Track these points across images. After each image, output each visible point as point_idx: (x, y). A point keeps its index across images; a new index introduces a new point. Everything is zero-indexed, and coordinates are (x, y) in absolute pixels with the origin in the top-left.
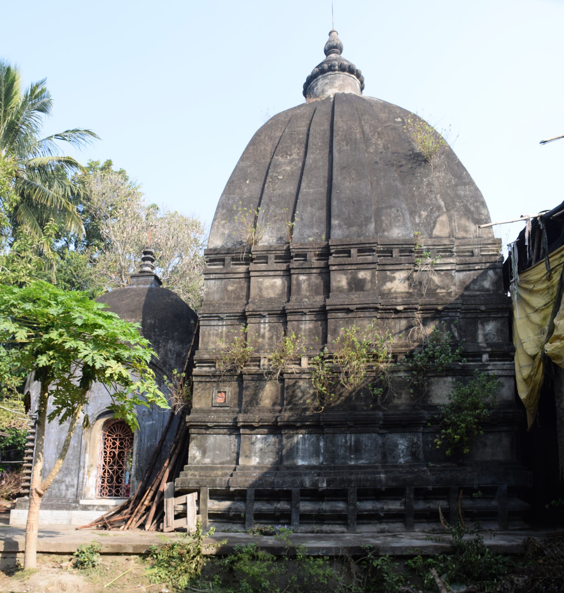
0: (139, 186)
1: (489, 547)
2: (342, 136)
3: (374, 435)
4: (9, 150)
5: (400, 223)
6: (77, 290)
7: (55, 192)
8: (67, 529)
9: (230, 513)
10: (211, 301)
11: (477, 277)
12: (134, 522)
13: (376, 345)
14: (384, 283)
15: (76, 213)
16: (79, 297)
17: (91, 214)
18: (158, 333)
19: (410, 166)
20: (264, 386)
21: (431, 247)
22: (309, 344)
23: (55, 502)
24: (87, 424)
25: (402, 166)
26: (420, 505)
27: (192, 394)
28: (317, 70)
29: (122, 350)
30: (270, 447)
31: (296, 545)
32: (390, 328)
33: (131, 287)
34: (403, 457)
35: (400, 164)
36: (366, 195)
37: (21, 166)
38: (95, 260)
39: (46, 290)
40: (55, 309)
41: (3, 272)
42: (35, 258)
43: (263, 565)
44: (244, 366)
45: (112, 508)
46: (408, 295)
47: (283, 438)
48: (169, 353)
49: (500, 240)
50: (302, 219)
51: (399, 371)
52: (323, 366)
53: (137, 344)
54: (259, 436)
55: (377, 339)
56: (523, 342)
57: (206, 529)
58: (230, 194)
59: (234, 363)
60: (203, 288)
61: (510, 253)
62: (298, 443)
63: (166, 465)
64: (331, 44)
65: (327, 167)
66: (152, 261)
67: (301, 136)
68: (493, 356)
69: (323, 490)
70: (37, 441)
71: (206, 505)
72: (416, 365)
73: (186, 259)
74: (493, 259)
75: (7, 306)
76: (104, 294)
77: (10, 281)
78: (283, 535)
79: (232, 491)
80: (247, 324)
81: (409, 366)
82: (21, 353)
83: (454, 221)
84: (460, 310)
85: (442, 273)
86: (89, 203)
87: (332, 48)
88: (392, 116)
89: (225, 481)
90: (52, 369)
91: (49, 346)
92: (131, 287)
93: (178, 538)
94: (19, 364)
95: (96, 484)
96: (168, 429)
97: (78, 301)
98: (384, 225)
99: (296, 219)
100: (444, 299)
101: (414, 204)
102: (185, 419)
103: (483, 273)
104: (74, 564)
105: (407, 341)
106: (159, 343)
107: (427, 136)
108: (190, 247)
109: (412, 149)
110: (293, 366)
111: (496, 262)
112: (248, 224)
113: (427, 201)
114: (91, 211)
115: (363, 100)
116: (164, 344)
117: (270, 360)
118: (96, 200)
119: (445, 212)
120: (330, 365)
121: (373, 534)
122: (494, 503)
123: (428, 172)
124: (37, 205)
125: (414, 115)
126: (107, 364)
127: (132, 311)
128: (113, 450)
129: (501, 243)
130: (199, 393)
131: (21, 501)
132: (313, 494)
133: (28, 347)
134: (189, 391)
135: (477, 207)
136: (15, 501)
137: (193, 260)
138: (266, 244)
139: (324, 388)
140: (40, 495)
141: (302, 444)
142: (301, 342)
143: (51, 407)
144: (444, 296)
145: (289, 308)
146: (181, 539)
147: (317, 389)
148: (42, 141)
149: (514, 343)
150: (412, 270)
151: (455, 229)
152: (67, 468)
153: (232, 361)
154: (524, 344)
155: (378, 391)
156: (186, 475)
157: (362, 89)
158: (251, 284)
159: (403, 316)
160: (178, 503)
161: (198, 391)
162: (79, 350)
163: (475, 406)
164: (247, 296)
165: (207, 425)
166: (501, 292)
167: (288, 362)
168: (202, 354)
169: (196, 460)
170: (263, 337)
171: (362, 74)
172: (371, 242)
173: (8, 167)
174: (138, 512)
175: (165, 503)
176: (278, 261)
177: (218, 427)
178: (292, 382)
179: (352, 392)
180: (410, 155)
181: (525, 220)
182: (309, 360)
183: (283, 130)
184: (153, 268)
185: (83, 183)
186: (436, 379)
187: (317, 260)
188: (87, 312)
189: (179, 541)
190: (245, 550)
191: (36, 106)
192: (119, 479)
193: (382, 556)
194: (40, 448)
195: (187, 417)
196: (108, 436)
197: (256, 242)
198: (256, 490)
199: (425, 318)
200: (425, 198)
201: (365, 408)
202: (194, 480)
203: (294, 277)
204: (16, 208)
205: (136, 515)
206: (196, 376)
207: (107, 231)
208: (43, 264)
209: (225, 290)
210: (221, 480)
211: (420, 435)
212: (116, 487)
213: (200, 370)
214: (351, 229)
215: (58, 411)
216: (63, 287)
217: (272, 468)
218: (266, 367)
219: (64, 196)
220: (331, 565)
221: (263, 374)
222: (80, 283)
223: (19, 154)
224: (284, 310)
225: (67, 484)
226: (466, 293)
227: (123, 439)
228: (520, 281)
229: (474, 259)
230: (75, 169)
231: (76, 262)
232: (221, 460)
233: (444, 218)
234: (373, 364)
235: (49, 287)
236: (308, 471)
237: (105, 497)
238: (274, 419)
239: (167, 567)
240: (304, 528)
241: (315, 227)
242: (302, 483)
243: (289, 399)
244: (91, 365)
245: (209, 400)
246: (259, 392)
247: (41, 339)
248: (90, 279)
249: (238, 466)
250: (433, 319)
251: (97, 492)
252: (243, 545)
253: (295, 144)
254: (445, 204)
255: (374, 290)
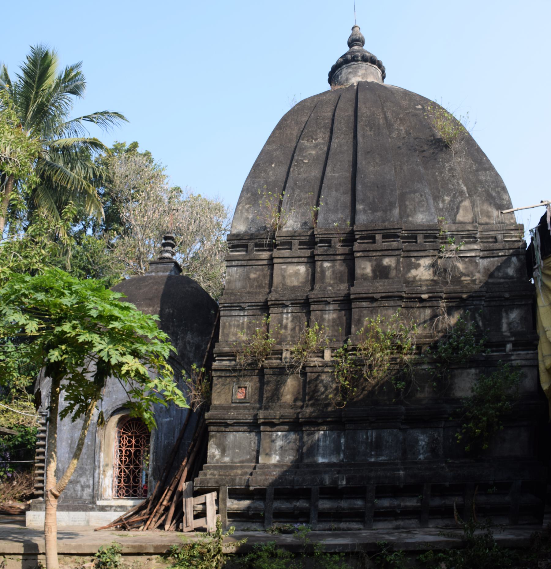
0: (163, 169)
1: (498, 541)
2: (365, 121)
3: (395, 430)
4: (35, 131)
5: (424, 208)
6: (92, 278)
7: (77, 174)
8: (86, 531)
9: (250, 512)
10: (232, 290)
11: (501, 264)
12: (153, 523)
13: (401, 335)
14: (409, 271)
15: (97, 195)
16: (94, 286)
17: (112, 196)
18: (176, 324)
19: (431, 151)
20: (286, 381)
21: (455, 233)
22: (332, 336)
23: (71, 503)
24: (102, 422)
25: (424, 151)
26: (436, 502)
27: (211, 390)
28: (341, 60)
29: (138, 345)
30: (291, 444)
31: (314, 542)
32: (415, 318)
33: (150, 274)
34: (422, 454)
35: (422, 149)
36: (390, 180)
37: (44, 147)
38: (113, 246)
39: (60, 278)
40: (69, 299)
41: (15, 259)
42: (50, 243)
43: (282, 562)
44: (266, 359)
45: (130, 509)
46: (433, 283)
47: (304, 435)
48: (187, 345)
49: (522, 225)
50: (327, 204)
51: (423, 363)
52: (346, 358)
53: (156, 337)
54: (279, 433)
55: (401, 330)
56: (546, 330)
57: (226, 528)
58: (255, 178)
59: (255, 356)
60: (224, 275)
61: (532, 239)
62: (319, 440)
63: (184, 464)
64: (354, 37)
65: (351, 152)
66: (173, 246)
67: (327, 121)
68: (516, 346)
69: (343, 488)
70: (48, 440)
71: (225, 504)
72: (440, 357)
73: (208, 245)
74: (516, 245)
75: (17, 296)
76: (121, 281)
77: (21, 268)
78: (301, 533)
79: (252, 491)
80: (269, 314)
81: (433, 358)
82: (31, 348)
83: (477, 207)
84: (484, 298)
85: (467, 260)
86: (111, 185)
87: (355, 41)
88: (412, 103)
89: (245, 480)
90: (63, 363)
91: (62, 338)
92: (150, 274)
93: (198, 538)
94: (28, 361)
95: (112, 485)
96: (186, 425)
97: (93, 290)
98: (408, 210)
99: (322, 204)
100: (469, 286)
101: (437, 189)
102: (204, 416)
103: (506, 259)
104: (96, 564)
105: (432, 332)
106: (177, 334)
107: (447, 122)
108: (213, 232)
109: (433, 135)
110: (316, 358)
111: (519, 248)
112: (272, 208)
113: (450, 186)
114: (112, 194)
115: (385, 88)
116: (182, 335)
117: (292, 353)
118: (118, 182)
119: (468, 198)
120: (354, 357)
121: (388, 530)
122: (507, 498)
123: (450, 157)
124: (56, 187)
125: (434, 102)
126: (124, 359)
127: (150, 299)
128: (129, 448)
129: (523, 229)
130: (218, 388)
131: (35, 503)
132: (333, 492)
133: (39, 341)
134: (208, 387)
135: (498, 193)
136: (28, 502)
137: (215, 245)
138: (290, 229)
139: (347, 382)
140: (56, 497)
141: (323, 441)
142: (324, 333)
143: (63, 403)
144: (468, 284)
145: (313, 296)
146: (201, 539)
147: (340, 383)
148: (69, 123)
149: (538, 331)
150: (437, 257)
151: (478, 215)
152: (81, 468)
153: (253, 353)
154: (547, 333)
155: (401, 385)
156: (205, 475)
157: (384, 77)
158: (275, 271)
159: (428, 305)
160: (196, 503)
161: (218, 386)
162: (94, 344)
163: (497, 399)
164: (269, 284)
165: (226, 423)
166: (524, 279)
167: (311, 354)
168: (222, 347)
169: (215, 459)
170: (286, 327)
171: (383, 65)
172: (396, 227)
173: (32, 148)
174: (156, 512)
175: (184, 503)
176: (302, 247)
177: (239, 424)
178: (315, 375)
179: (374, 386)
180: (432, 141)
181: (545, 205)
182: (332, 352)
183: (309, 115)
184: (173, 254)
185: (106, 164)
186: (459, 371)
187: (342, 246)
188: (103, 303)
189: (200, 541)
190: (264, 548)
191: (68, 89)
192: (136, 479)
193: (395, 551)
194: (52, 447)
195: (206, 415)
196: (123, 433)
197: (280, 227)
198: (275, 489)
199: (450, 307)
200: (447, 184)
201: (388, 403)
202: (213, 480)
203: (319, 263)
204: (35, 190)
205: (155, 516)
206: (216, 370)
207: (128, 214)
208: (58, 249)
209: (247, 277)
210: (240, 479)
211: (441, 430)
212: (133, 487)
213: (220, 364)
214: (375, 214)
215: (71, 408)
216: (78, 274)
217: (292, 466)
218: (288, 360)
219: (85, 178)
220: (346, 561)
221: (285, 368)
222: (95, 270)
223: (44, 135)
224: (307, 299)
225: (83, 484)
226: (491, 281)
227: (139, 437)
228: (544, 267)
229: (498, 246)
230: (99, 151)
231: (92, 248)
232: (241, 459)
233: (466, 203)
234: (397, 356)
235: (63, 275)
236: (327, 469)
237: (122, 497)
238: (295, 415)
239: (188, 566)
240: (321, 526)
241: (340, 212)
242: (322, 480)
243: (311, 394)
244: (106, 360)
245: (231, 395)
246: (280, 387)
247: (52, 332)
248: (106, 266)
249: (258, 465)
250: (457, 308)
251: (114, 492)
252: (262, 543)
253: (320, 129)
254: (467, 189)
255: (399, 278)
